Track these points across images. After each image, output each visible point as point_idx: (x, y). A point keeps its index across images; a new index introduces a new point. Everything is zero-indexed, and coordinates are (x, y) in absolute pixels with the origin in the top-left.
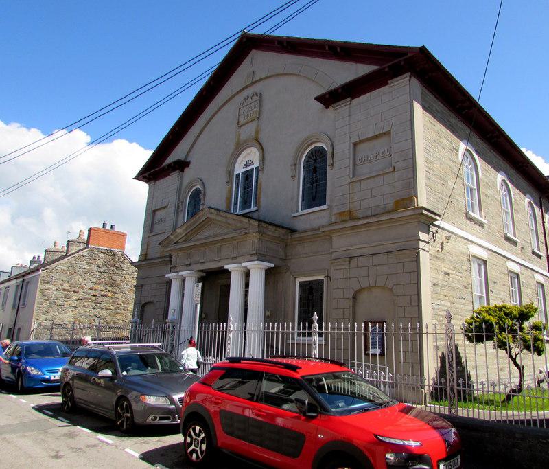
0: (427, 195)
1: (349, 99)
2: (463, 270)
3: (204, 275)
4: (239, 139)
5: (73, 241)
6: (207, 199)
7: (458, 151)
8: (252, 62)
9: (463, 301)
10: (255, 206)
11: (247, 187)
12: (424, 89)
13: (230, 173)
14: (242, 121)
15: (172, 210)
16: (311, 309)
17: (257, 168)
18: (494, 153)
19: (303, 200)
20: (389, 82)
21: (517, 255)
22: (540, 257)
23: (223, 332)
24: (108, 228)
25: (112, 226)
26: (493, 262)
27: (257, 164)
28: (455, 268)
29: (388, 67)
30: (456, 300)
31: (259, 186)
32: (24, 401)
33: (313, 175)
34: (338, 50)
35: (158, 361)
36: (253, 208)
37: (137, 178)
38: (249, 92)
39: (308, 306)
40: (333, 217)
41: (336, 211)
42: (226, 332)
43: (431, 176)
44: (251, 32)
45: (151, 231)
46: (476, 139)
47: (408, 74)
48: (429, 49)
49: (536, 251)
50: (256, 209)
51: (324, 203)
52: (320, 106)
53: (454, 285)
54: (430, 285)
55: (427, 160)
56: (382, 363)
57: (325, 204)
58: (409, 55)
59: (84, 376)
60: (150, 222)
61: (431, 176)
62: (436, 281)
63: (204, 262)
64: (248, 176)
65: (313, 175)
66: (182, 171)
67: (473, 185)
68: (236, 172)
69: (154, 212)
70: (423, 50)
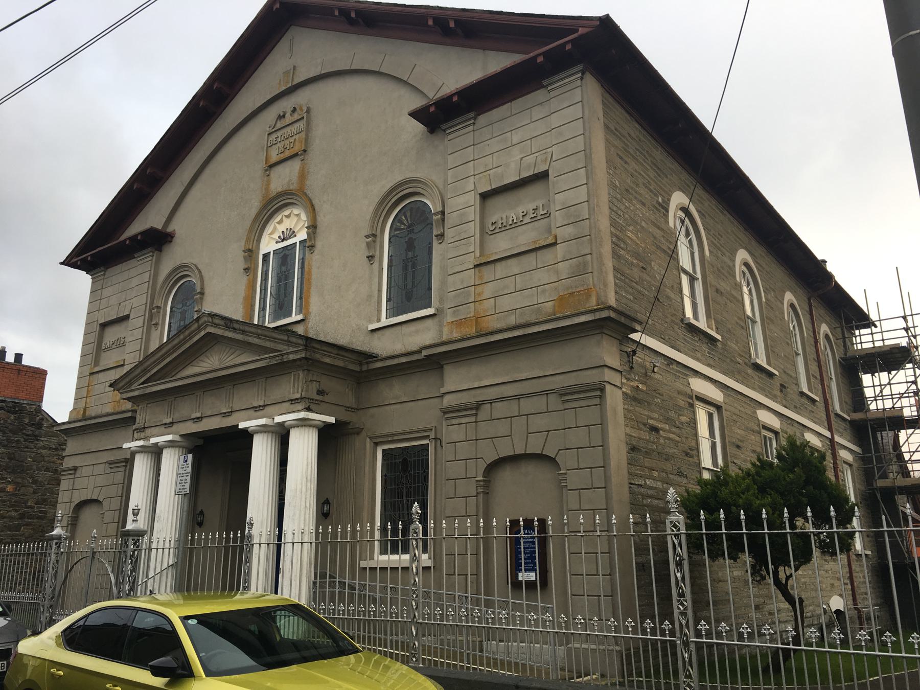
1: (472, 115)
2: (682, 423)
3: (200, 442)
4: (267, 189)
6: (208, 298)
8: (291, 50)
10: (300, 311)
11: (284, 278)
12: (607, 96)
13: (250, 253)
14: (274, 158)
15: (137, 322)
16: (405, 499)
18: (728, 215)
19: (388, 300)
21: (774, 398)
22: (813, 401)
23: (234, 548)
25: (19, 357)
26: (732, 409)
27: (302, 235)
28: (668, 420)
29: (544, 54)
31: (306, 276)
33: (407, 254)
34: (452, 25)
35: (892, 662)
36: (295, 317)
37: (70, 262)
38: (285, 105)
39: (400, 495)
40: (446, 330)
41: (449, 318)
42: (241, 547)
43: (622, 252)
45: (97, 363)
46: (700, 191)
49: (806, 390)
50: (300, 317)
52: (417, 127)
53: (667, 450)
54: (624, 449)
55: (614, 223)
57: (430, 306)
58: (581, 31)
60: (92, 348)
61: (622, 252)
63: (200, 419)
64: (285, 256)
65: (407, 254)
66: (160, 250)
68: (263, 250)
69: (104, 326)
70: (606, 23)
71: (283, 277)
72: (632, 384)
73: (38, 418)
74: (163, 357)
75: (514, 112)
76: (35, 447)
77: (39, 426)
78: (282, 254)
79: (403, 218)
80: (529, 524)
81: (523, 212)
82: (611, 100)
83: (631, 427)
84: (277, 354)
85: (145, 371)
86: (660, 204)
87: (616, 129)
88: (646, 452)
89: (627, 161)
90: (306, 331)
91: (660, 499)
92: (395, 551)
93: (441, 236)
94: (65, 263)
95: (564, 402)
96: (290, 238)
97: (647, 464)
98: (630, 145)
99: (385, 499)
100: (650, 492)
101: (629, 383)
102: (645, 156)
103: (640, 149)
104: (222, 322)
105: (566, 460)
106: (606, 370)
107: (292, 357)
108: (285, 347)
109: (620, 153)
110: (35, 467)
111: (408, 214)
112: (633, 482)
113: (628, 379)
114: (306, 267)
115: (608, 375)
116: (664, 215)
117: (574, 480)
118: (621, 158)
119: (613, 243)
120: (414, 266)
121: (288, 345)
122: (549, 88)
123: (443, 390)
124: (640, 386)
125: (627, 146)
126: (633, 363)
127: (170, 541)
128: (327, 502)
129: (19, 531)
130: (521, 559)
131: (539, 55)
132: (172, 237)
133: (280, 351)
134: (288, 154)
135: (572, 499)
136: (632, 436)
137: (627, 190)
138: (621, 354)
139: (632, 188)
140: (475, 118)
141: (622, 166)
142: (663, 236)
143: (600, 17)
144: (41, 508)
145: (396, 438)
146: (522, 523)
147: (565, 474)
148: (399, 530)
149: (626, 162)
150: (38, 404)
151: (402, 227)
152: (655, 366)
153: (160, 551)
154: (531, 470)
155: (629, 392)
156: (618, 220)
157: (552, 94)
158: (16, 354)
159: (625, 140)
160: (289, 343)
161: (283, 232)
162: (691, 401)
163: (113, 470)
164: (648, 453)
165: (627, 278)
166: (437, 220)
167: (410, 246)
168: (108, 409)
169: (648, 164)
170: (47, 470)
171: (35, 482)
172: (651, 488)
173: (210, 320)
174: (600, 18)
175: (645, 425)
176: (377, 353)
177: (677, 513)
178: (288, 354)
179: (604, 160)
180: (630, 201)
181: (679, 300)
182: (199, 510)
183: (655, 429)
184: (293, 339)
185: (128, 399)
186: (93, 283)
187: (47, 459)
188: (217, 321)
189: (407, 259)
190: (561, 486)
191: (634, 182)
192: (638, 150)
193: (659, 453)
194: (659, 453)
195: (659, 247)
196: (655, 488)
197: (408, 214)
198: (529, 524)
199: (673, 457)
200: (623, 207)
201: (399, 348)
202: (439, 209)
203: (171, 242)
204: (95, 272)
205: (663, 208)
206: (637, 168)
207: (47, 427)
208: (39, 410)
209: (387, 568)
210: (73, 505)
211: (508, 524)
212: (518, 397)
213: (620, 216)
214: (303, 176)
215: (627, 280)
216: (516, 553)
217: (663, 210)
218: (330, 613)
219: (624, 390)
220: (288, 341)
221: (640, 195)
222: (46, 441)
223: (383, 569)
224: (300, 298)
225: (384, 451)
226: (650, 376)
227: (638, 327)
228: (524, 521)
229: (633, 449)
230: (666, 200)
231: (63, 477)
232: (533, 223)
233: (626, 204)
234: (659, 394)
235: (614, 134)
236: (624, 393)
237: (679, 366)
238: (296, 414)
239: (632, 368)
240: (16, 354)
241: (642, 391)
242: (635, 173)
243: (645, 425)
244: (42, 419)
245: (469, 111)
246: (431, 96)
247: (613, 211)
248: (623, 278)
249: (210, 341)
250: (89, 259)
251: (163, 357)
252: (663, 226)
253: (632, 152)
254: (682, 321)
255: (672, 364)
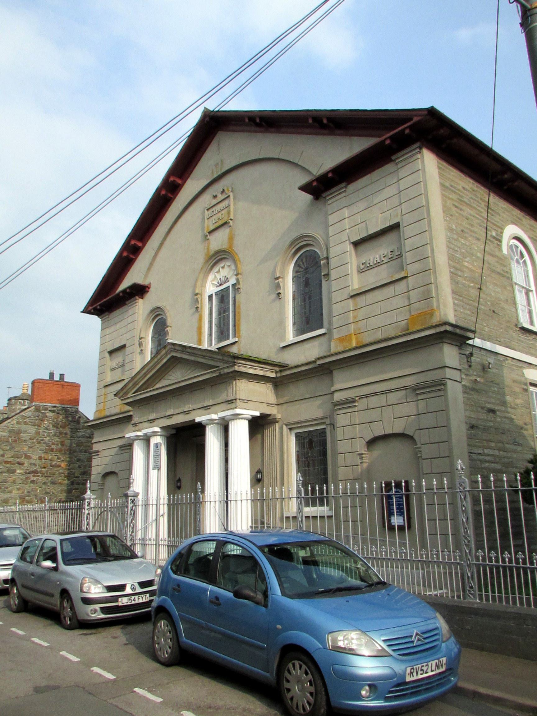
0: (454, 304)
1: (343, 185)
2: (517, 405)
4: (208, 249)
5: (15, 398)
7: (500, 241)
9: (519, 448)
10: (234, 336)
13: (196, 297)
17: (234, 285)
20: (393, 158)
24: (57, 378)
25: (62, 376)
27: (233, 281)
29: (390, 137)
30: (507, 446)
31: (237, 310)
32: (21, 632)
34: (325, 121)
36: (231, 340)
37: (86, 311)
39: (309, 466)
43: (459, 279)
44: (223, 109)
47: (418, 144)
48: (436, 107)
51: (321, 327)
52: (308, 197)
54: (464, 428)
55: (451, 258)
56: (402, 537)
58: (415, 119)
59: (393, 524)
61: (459, 279)
62: (474, 422)
67: (530, 287)
70: (432, 112)
71: (222, 312)
72: (472, 378)
73: (77, 417)
74: (145, 374)
75: (373, 181)
76: (77, 437)
77: (78, 422)
78: (221, 295)
79: (301, 263)
80: (398, 485)
81: (383, 254)
82: (445, 164)
83: (470, 411)
84: (216, 369)
85: (135, 384)
86: (494, 238)
87: (451, 186)
88: (484, 428)
89: (462, 208)
90: (239, 350)
91: (497, 463)
92: (314, 505)
93: (327, 275)
94: (83, 312)
95: (418, 394)
96: (225, 282)
97: (484, 438)
98: (464, 195)
99: (299, 468)
100: (488, 458)
101: (468, 377)
102: (478, 202)
103: (474, 198)
104: (180, 348)
105: (421, 437)
106: (447, 369)
107: (226, 371)
108: (222, 364)
109: (456, 204)
110: (78, 450)
111: (304, 260)
112: (472, 451)
113: (467, 375)
114: (237, 303)
115: (449, 373)
116: (498, 245)
117: (426, 451)
118: (456, 207)
119: (451, 272)
120: (310, 298)
121: (223, 363)
122: (397, 161)
123: (333, 389)
124: (478, 379)
125: (462, 197)
126: (471, 362)
127: (164, 499)
128: (259, 472)
129: (71, 493)
130: (393, 509)
131: (386, 139)
132: (149, 288)
133: (219, 367)
134: (221, 223)
135: (425, 466)
136: (471, 417)
137: (462, 231)
138: (460, 357)
139: (467, 228)
140: (346, 187)
141: (457, 213)
142: (497, 262)
143: (427, 109)
144: (84, 477)
145: (303, 425)
146: (393, 484)
147: (419, 448)
148: (491, 482)
149: (461, 210)
150: (76, 407)
151: (301, 270)
152: (489, 364)
153: (239, 502)
154: (395, 444)
155: (467, 384)
156: (456, 255)
157: (400, 165)
158: (60, 375)
159: (459, 193)
160: (223, 361)
161: (220, 279)
162: (525, 387)
163: (122, 452)
164: (486, 429)
165: (464, 298)
166: (324, 264)
167: (307, 283)
168: (117, 410)
169: (482, 208)
170: (85, 452)
171: (79, 460)
172: (488, 455)
173: (173, 347)
174: (427, 110)
175: (483, 408)
176: (288, 363)
177: (463, 477)
178: (223, 368)
179: (441, 211)
180: (466, 238)
181: (513, 310)
182: (178, 478)
183: (492, 411)
184: (226, 358)
185: (126, 404)
186: (102, 323)
187: (85, 444)
188: (177, 348)
189: (306, 293)
190: (417, 457)
191: (469, 224)
192: (472, 198)
193: (496, 429)
194: (496, 429)
195: (493, 271)
196: (493, 455)
197: (304, 260)
198: (398, 485)
199: (509, 431)
200: (459, 245)
201: (302, 359)
202: (325, 256)
203: (148, 291)
204: (103, 316)
205: (497, 239)
206: (472, 212)
207: (83, 423)
208: (77, 411)
209: (316, 517)
210: (101, 475)
211: (383, 485)
212: (386, 392)
213: (457, 251)
214: (231, 239)
215: (464, 300)
216: (390, 505)
217: (496, 242)
218: (373, 554)
219: (463, 383)
220: (223, 360)
221: (475, 233)
222: (83, 432)
223: (315, 517)
224: (234, 326)
225: (296, 434)
226: (486, 371)
227: (471, 335)
228: (395, 483)
229: (472, 427)
230: (499, 233)
231: (93, 457)
232: (391, 263)
233: (463, 242)
234: (496, 384)
235: (450, 189)
236: (463, 386)
237: (514, 361)
238: (231, 411)
239: (470, 366)
240: (60, 375)
241: (479, 382)
242: (470, 217)
243: (483, 408)
244: (80, 417)
245: (340, 182)
246: (315, 173)
247: (451, 248)
248: (461, 298)
249: (174, 362)
250: (98, 307)
251: (145, 374)
252: (497, 254)
253: (467, 201)
254: (516, 325)
255: (507, 360)
